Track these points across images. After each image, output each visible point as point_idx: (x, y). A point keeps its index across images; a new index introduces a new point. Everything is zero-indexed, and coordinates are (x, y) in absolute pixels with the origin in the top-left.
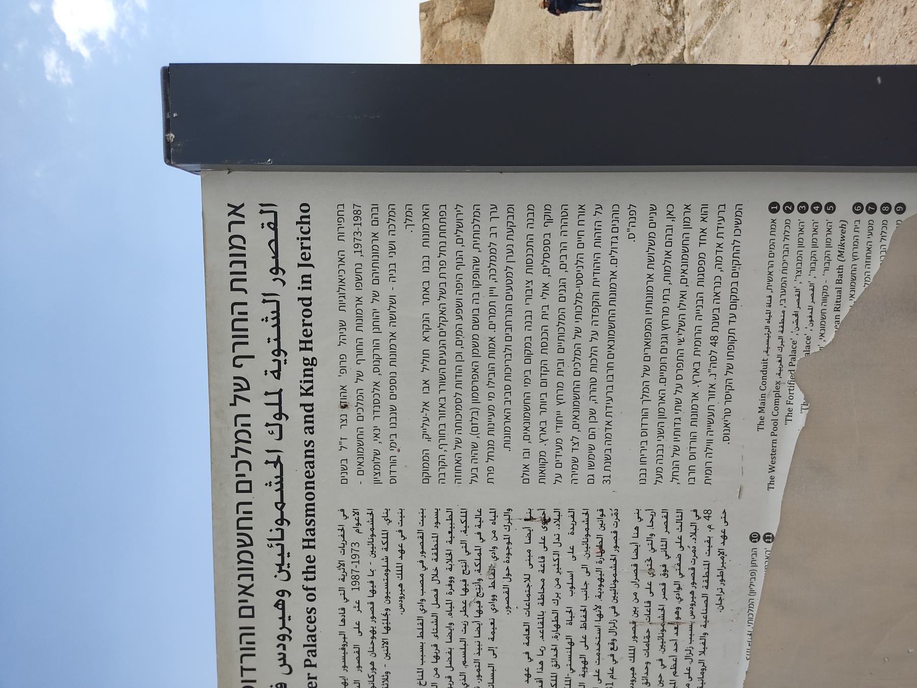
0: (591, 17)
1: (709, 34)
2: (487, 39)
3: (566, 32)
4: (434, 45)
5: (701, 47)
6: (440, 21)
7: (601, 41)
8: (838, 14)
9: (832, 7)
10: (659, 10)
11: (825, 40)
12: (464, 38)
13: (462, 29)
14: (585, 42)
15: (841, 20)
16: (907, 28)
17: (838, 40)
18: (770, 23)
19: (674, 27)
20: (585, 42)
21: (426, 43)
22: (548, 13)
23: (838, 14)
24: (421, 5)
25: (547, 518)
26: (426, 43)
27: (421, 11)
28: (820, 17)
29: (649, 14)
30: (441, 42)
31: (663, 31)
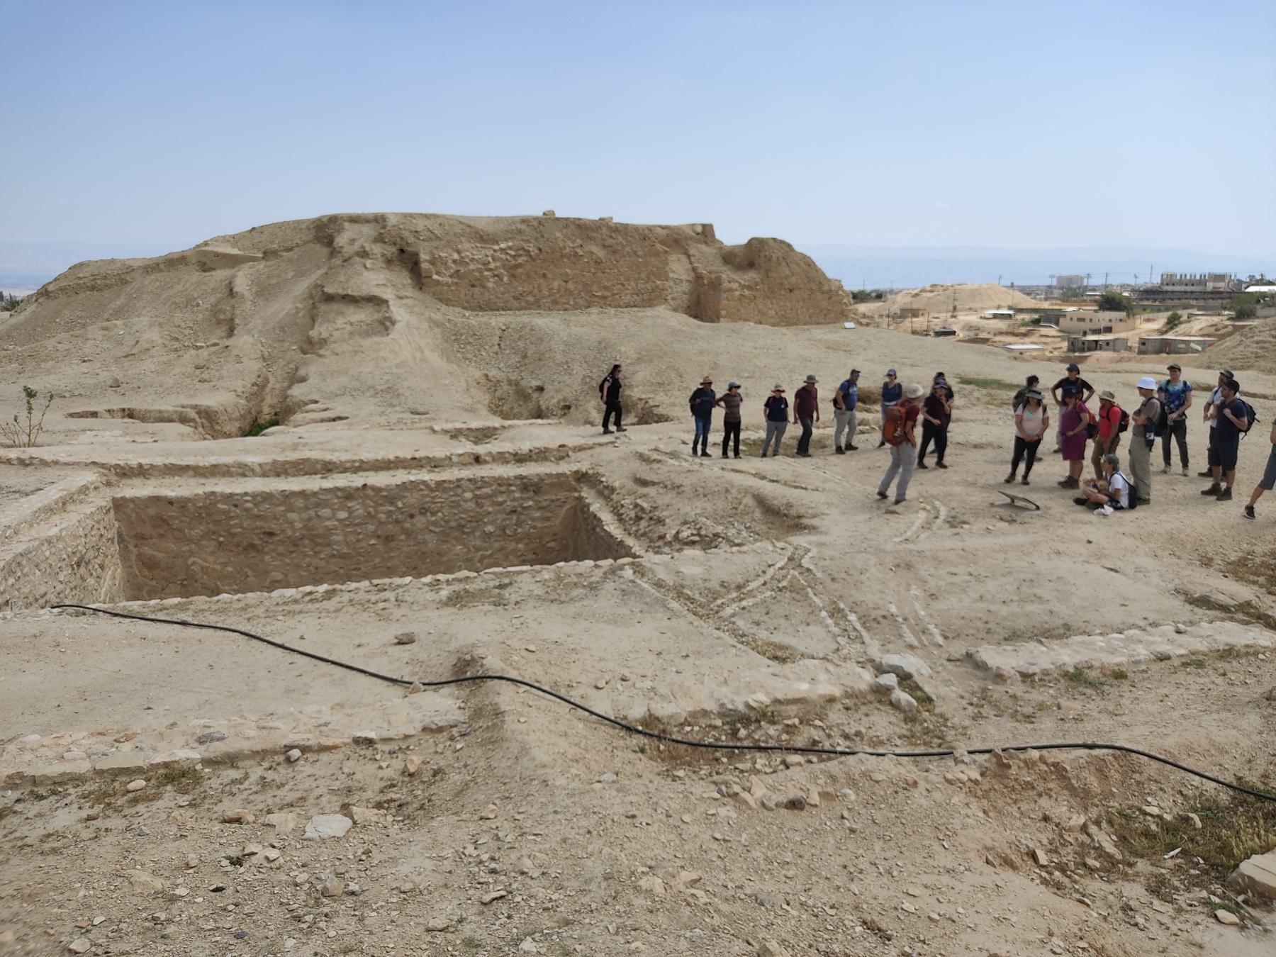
0: (684, 443)
1: (646, 586)
2: (669, 314)
3: (671, 414)
4: (663, 243)
5: (632, 577)
6: (692, 252)
7: (655, 456)
8: (651, 736)
9: (661, 727)
10: (685, 523)
11: (623, 726)
12: (672, 283)
13: (681, 281)
14: (655, 437)
15: (643, 740)
16: (610, 822)
17: (622, 743)
18: (651, 657)
19: (666, 544)
20: (655, 437)
21: (665, 232)
22: (694, 389)
23: (651, 736)
24: (711, 226)
25: (302, 372)
26: (665, 232)
27: (704, 226)
28: (651, 715)
29: (682, 511)
30: (666, 252)
31: (661, 530)
